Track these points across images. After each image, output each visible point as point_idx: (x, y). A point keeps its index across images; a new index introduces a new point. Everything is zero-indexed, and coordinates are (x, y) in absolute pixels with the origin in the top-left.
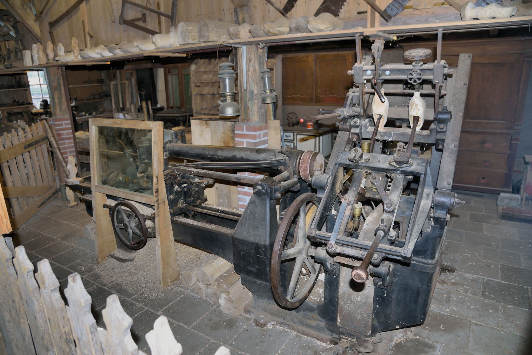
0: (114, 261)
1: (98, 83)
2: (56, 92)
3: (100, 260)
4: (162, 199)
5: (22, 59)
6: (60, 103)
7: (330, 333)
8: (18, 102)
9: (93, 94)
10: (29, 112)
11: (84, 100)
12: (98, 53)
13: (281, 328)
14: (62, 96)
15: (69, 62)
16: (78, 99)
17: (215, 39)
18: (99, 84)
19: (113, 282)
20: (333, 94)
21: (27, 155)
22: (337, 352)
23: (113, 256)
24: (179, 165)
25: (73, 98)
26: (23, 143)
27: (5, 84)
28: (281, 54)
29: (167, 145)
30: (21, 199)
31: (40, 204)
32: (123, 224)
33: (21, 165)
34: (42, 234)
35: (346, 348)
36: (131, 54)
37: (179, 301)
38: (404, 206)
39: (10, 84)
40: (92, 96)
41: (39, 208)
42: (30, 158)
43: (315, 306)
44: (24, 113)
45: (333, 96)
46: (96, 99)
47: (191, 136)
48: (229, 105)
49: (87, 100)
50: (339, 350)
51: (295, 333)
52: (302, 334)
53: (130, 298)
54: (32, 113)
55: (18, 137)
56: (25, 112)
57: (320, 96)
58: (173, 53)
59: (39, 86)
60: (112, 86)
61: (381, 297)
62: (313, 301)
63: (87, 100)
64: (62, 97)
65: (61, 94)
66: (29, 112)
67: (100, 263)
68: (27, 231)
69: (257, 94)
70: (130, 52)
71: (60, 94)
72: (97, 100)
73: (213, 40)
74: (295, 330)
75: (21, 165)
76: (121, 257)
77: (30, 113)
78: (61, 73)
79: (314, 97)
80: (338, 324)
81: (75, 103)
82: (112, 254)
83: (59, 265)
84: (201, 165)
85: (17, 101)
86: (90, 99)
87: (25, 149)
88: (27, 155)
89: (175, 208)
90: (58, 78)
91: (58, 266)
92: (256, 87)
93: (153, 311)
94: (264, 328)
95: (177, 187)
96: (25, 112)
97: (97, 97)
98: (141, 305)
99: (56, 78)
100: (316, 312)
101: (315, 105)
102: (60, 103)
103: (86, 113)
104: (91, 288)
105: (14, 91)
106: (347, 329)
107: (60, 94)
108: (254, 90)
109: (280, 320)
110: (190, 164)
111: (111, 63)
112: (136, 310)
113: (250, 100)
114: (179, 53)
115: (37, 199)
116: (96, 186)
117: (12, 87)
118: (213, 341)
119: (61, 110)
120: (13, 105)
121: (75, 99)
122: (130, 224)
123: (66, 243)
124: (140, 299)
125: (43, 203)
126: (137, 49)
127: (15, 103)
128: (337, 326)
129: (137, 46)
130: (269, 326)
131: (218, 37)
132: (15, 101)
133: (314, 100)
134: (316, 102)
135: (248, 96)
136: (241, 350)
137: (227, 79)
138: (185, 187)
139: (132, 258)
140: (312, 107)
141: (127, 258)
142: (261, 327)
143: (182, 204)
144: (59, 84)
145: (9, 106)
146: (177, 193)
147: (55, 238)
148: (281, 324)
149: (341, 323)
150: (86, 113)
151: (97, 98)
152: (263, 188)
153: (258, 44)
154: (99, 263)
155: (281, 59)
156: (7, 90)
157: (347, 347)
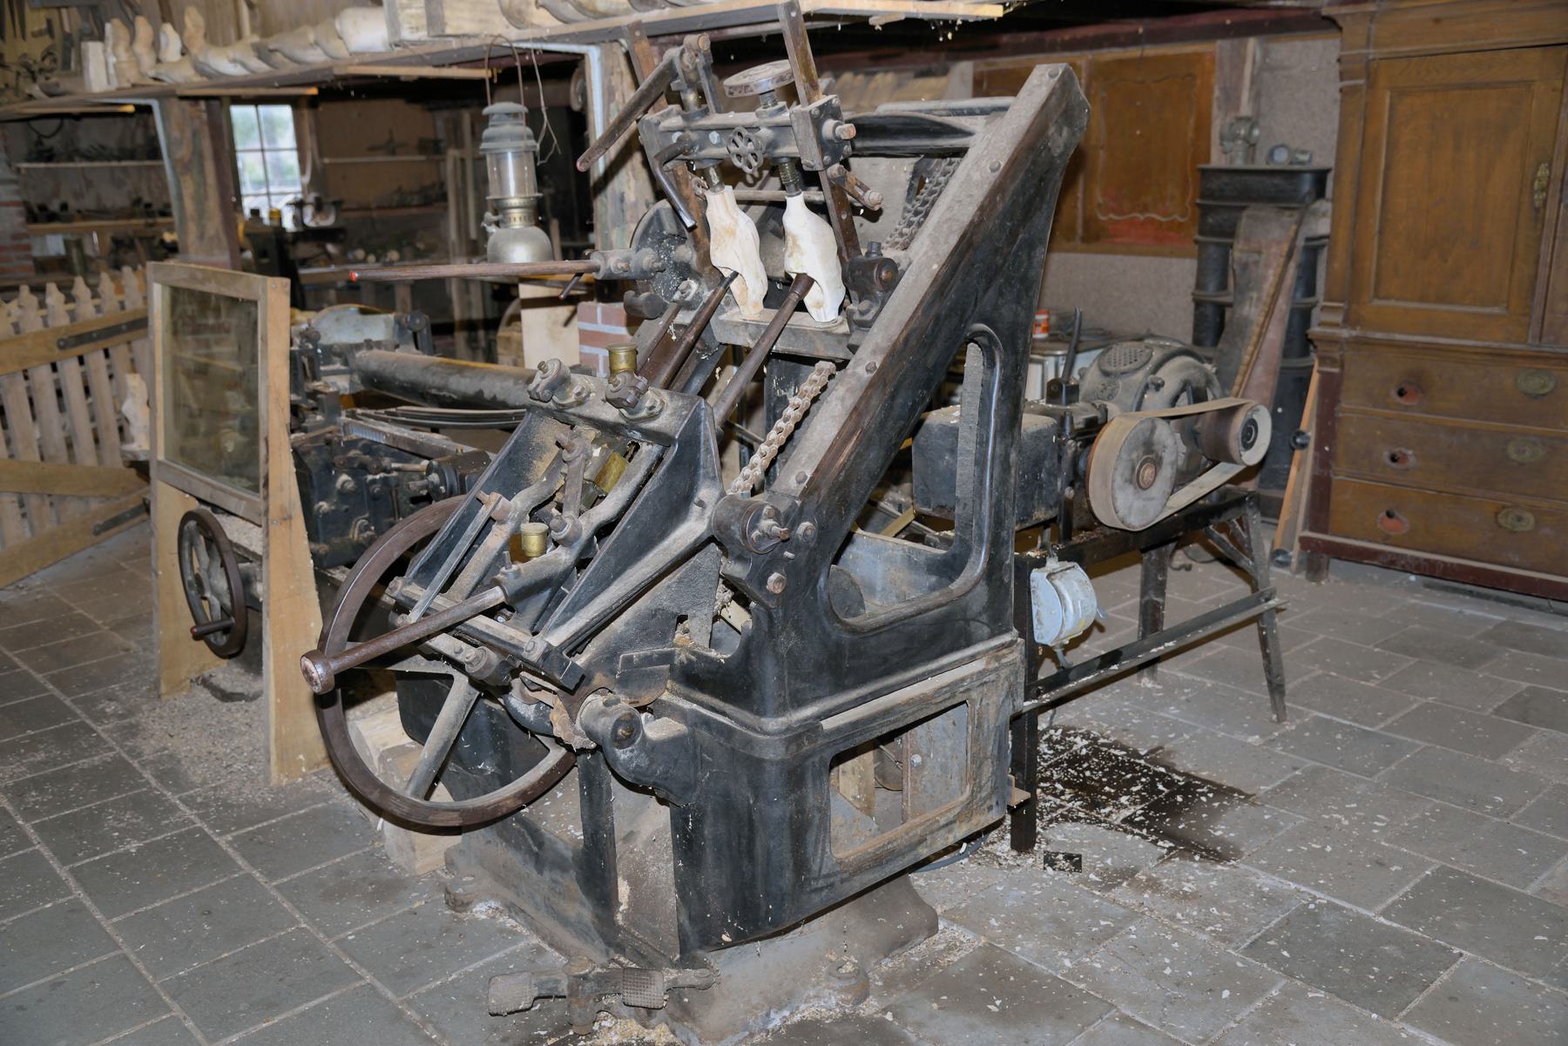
0: (204, 694)
1: (421, 154)
2: (188, 178)
3: (163, 688)
4: (282, 509)
5: (80, 72)
6: (201, 214)
7: (603, 946)
8: (148, 206)
9: (399, 190)
10: (153, 238)
11: (367, 208)
12: (234, 61)
13: (510, 923)
14: (206, 191)
15: (178, 85)
16: (344, 206)
17: (468, 28)
18: (422, 158)
19: (165, 749)
20: (1145, 209)
21: (71, 372)
22: (550, 985)
23: (206, 683)
24: (363, 415)
25: (331, 200)
26: (57, 330)
27: (112, 143)
28: (967, 58)
29: (358, 355)
30: (33, 501)
31: (100, 522)
32: (667, 667)
33: (47, 400)
34: (71, 609)
35: (581, 976)
36: (307, 68)
37: (300, 817)
38: (901, 575)
39: (128, 145)
40: (396, 198)
41: (97, 533)
42: (111, 377)
43: (569, 854)
44: (137, 242)
45: (1142, 217)
46: (410, 206)
47: (521, 331)
48: (518, 237)
49: (380, 208)
50: (558, 981)
51: (535, 940)
52: (551, 945)
53: (177, 792)
54: (162, 242)
55: (43, 312)
56: (141, 239)
57: (1102, 218)
58: (436, 66)
59: (259, 155)
60: (450, 166)
61: (685, 832)
62: (566, 839)
63: (380, 208)
64: (206, 198)
65: (205, 184)
66: (153, 238)
67: (164, 698)
68: (39, 596)
69: (635, 204)
70: (307, 63)
71: (202, 184)
72: (414, 211)
73: (460, 32)
74: (537, 931)
75: (47, 400)
76: (226, 685)
77: (156, 242)
78: (205, 116)
79: (1080, 221)
80: (619, 917)
81: (337, 219)
82: (206, 674)
83: (57, 693)
84: (403, 415)
85: (147, 199)
86: (390, 207)
87: (61, 348)
88: (71, 372)
89: (336, 540)
90: (195, 134)
91: (52, 696)
92: (632, 182)
93: (210, 832)
94: (461, 915)
95: (344, 477)
96: (141, 239)
97: (416, 200)
98: (190, 814)
99: (188, 134)
100: (573, 874)
101: (1082, 251)
102: (201, 214)
103: (367, 254)
104: (96, 758)
105: (139, 168)
106: (633, 936)
107: (202, 184)
108: (625, 189)
109: (511, 896)
110: (383, 411)
111: (320, 90)
112: (167, 825)
113: (614, 225)
114: (459, 64)
115: (95, 505)
116: (160, 463)
117: (131, 156)
118: (304, 926)
119: (201, 236)
120: (132, 216)
121: (337, 204)
122: (209, 577)
123: (118, 639)
124: (199, 800)
125: (115, 522)
126: (319, 51)
127: (137, 209)
128: (614, 923)
129: (317, 43)
130: (481, 910)
131: (481, 21)
132: (138, 201)
133: (1080, 231)
134: (1085, 240)
135: (611, 210)
136: (353, 958)
137: (510, 155)
138: (374, 481)
139: (252, 691)
140: (1072, 256)
141: (239, 690)
142: (454, 909)
143: (361, 532)
144: (198, 154)
145: (117, 218)
146: (344, 495)
147: (100, 622)
148: (512, 909)
149: (626, 916)
150: (367, 254)
151: (415, 202)
152: (443, 482)
153: (616, 41)
154: (159, 697)
155: (969, 78)
156: (114, 164)
157: (585, 977)
